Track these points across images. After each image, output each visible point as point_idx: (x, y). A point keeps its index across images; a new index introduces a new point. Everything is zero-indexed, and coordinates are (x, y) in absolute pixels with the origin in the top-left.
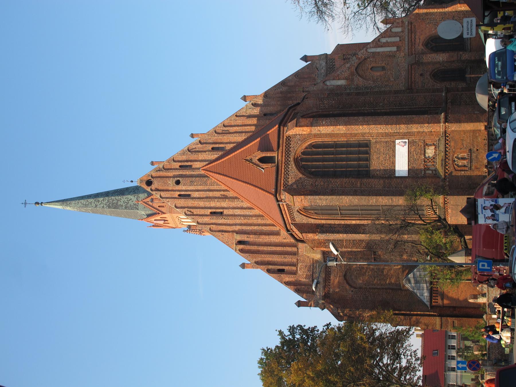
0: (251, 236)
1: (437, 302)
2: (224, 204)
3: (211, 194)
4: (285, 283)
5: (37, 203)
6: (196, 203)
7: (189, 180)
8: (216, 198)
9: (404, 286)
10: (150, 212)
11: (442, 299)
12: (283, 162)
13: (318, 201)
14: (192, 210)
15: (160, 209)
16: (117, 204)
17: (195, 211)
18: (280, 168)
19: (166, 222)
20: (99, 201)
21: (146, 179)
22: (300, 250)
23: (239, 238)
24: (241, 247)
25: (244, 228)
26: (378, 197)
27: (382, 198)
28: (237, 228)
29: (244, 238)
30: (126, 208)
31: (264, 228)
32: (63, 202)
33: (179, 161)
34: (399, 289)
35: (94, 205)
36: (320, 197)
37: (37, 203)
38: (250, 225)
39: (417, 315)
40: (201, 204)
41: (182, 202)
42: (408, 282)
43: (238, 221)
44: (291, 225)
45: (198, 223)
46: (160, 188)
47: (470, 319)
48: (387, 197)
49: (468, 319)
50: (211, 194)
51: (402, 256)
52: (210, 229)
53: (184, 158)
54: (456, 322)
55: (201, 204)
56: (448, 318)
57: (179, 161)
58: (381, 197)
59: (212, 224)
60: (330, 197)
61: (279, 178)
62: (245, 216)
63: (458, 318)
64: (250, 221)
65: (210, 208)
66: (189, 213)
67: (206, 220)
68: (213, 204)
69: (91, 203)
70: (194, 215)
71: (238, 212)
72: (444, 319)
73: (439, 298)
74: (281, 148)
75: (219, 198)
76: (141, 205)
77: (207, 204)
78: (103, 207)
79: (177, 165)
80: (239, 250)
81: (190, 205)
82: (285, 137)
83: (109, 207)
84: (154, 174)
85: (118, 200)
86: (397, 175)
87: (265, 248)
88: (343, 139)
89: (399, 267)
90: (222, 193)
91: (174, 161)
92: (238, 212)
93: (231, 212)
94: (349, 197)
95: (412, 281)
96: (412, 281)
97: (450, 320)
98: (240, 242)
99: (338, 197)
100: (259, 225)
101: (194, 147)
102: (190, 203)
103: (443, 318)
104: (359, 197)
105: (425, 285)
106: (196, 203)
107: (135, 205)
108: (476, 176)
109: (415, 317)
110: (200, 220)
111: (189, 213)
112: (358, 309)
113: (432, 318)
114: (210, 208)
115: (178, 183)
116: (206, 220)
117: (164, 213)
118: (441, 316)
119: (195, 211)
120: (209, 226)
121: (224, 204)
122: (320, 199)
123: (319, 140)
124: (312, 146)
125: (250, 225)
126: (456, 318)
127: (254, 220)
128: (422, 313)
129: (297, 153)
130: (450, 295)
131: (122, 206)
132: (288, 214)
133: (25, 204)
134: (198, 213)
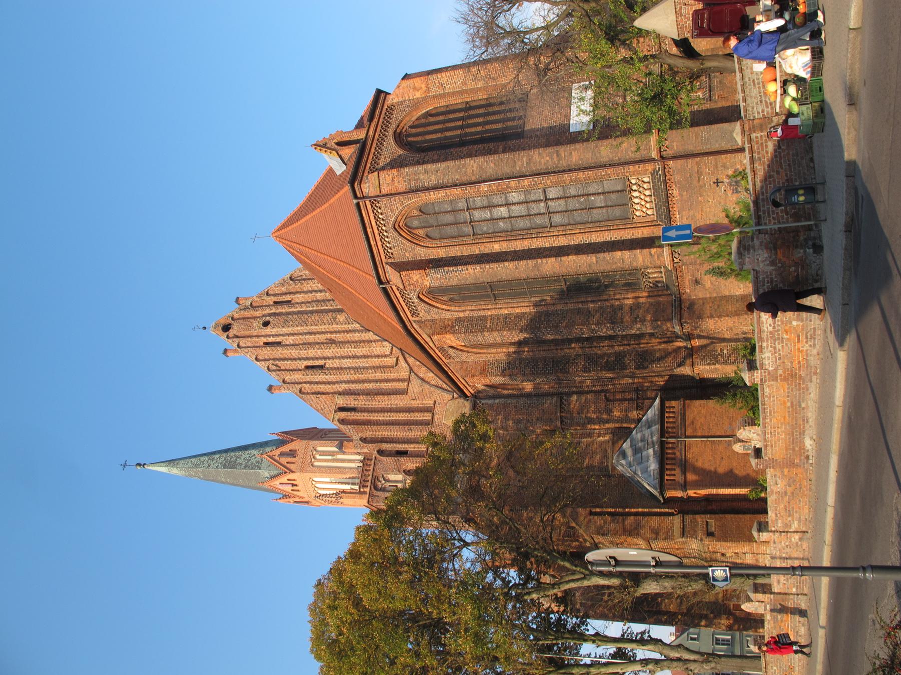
0: (361, 397)
1: (674, 475)
2: (328, 352)
3: (311, 338)
4: (404, 471)
5: (139, 464)
6: (287, 352)
7: (281, 319)
8: (317, 343)
9: (614, 468)
10: (276, 472)
11: (684, 472)
12: (376, 138)
13: (422, 177)
14: (278, 363)
15: (288, 465)
16: (235, 462)
17: (283, 364)
18: (368, 146)
19: (295, 488)
20: (213, 459)
21: (223, 322)
22: (436, 417)
23: (341, 401)
24: (343, 415)
25: (353, 386)
26: (531, 153)
27: (539, 154)
28: (344, 386)
29: (350, 402)
30: (245, 467)
31: (384, 386)
32: (171, 462)
33: (274, 295)
34: (606, 472)
35: (206, 464)
36: (425, 166)
37: (139, 464)
38: (363, 381)
39: (636, 514)
40: (295, 353)
41: (267, 352)
42: (621, 457)
43: (345, 377)
44: (388, 268)
45: (284, 381)
46: (242, 333)
47: (741, 516)
48: (549, 150)
49: (736, 516)
50: (311, 338)
51: (611, 411)
52: (300, 391)
53: (283, 289)
54: (712, 522)
55: (295, 353)
56: (697, 516)
57: (274, 295)
58: (536, 151)
59: (305, 383)
60: (442, 166)
61: (365, 159)
62: (356, 369)
63: (717, 516)
64: (362, 377)
65: (307, 359)
66: (275, 368)
67: (297, 377)
68: (311, 353)
69: (203, 462)
70: (279, 370)
71: (347, 363)
72: (688, 518)
73: (678, 472)
74: (375, 120)
75: (322, 343)
76: (266, 460)
77: (303, 353)
78: (217, 467)
79: (270, 300)
80: (338, 420)
81: (278, 356)
82: (386, 107)
83: (225, 467)
84: (236, 316)
85: (237, 457)
86: (572, 130)
87: (380, 417)
88: (481, 96)
89: (607, 438)
90: (328, 336)
91: (267, 294)
92: (347, 363)
93: (336, 363)
94: (477, 159)
95: (629, 452)
96: (629, 452)
97: (700, 519)
98: (342, 409)
99: (458, 163)
100: (376, 381)
101: (300, 274)
102: (278, 352)
103: (686, 517)
104: (496, 157)
105: (651, 451)
106: (287, 352)
107: (258, 462)
108: (723, 108)
109: (632, 518)
110: (289, 377)
111: (275, 368)
112: (526, 507)
113: (666, 518)
114: (307, 359)
115: (266, 324)
116: (297, 377)
117: (293, 472)
118: (683, 512)
119: (283, 364)
120: (300, 386)
121: (328, 352)
122: (426, 172)
123: (443, 103)
124: (428, 114)
125: (363, 381)
126: (713, 516)
127: (371, 375)
128: (646, 510)
129: (402, 125)
130: (699, 464)
131: (241, 464)
132: (401, 300)
133: (125, 465)
134: (288, 367)
